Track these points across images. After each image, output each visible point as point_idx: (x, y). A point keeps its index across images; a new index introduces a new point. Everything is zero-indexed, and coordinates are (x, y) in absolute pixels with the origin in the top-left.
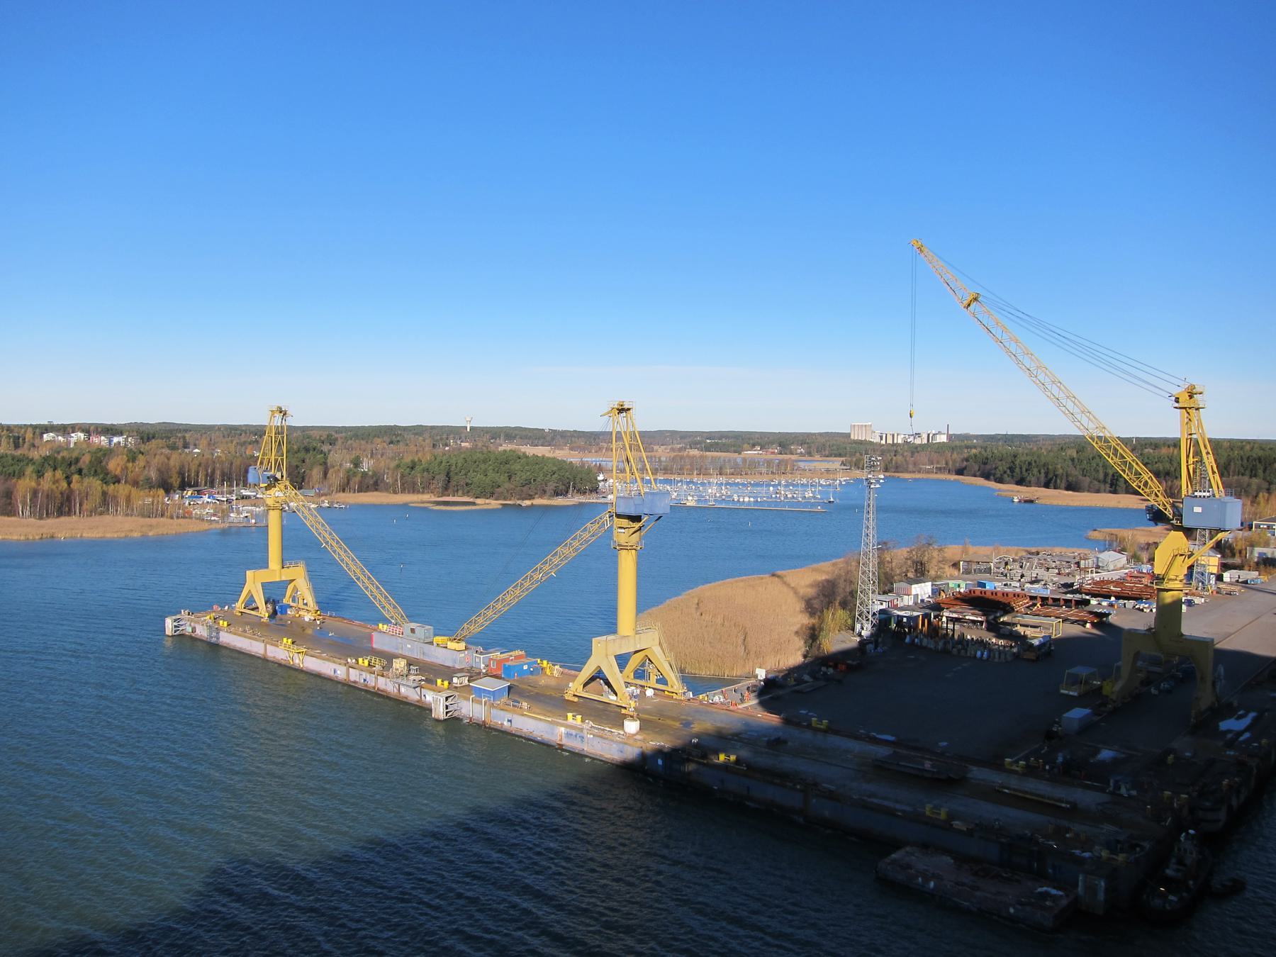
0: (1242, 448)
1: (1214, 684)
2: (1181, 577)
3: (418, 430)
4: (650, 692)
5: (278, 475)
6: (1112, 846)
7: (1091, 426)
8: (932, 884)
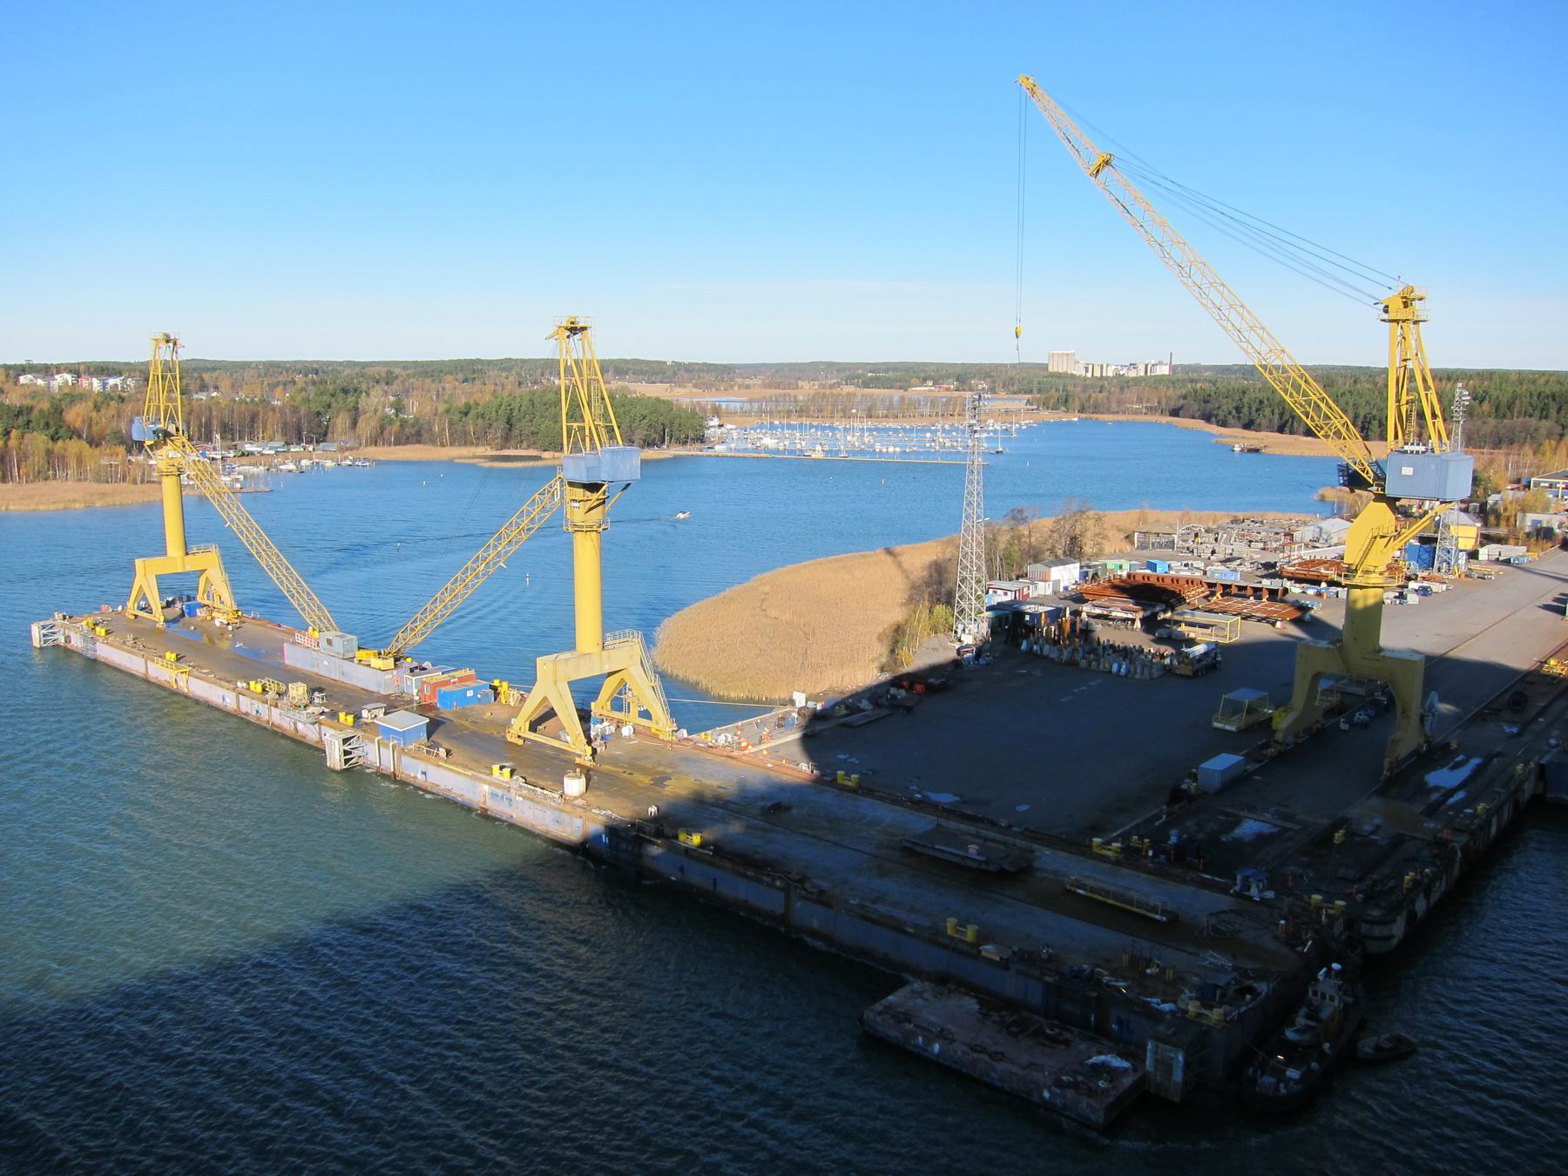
0: (1534, 382)
1: (1422, 719)
2: (1383, 568)
3: (506, 365)
4: (626, 731)
5: (172, 429)
6: (1207, 996)
7: (1264, 349)
8: (937, 1047)
